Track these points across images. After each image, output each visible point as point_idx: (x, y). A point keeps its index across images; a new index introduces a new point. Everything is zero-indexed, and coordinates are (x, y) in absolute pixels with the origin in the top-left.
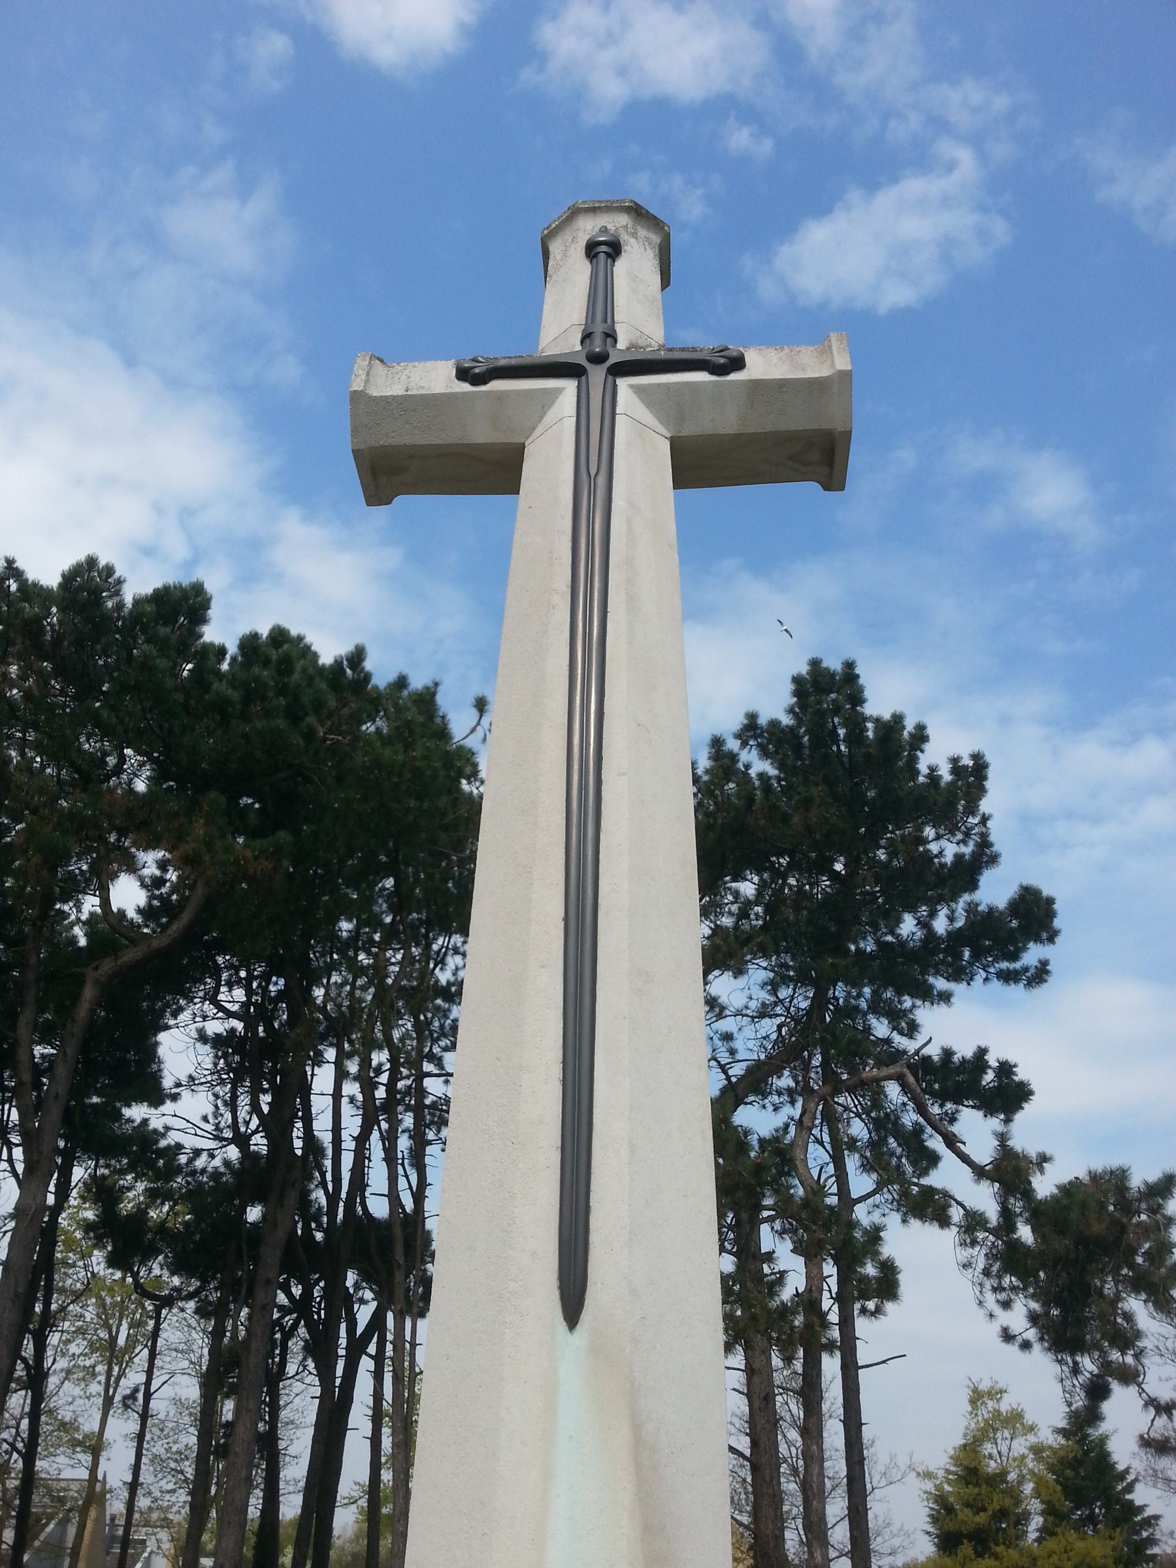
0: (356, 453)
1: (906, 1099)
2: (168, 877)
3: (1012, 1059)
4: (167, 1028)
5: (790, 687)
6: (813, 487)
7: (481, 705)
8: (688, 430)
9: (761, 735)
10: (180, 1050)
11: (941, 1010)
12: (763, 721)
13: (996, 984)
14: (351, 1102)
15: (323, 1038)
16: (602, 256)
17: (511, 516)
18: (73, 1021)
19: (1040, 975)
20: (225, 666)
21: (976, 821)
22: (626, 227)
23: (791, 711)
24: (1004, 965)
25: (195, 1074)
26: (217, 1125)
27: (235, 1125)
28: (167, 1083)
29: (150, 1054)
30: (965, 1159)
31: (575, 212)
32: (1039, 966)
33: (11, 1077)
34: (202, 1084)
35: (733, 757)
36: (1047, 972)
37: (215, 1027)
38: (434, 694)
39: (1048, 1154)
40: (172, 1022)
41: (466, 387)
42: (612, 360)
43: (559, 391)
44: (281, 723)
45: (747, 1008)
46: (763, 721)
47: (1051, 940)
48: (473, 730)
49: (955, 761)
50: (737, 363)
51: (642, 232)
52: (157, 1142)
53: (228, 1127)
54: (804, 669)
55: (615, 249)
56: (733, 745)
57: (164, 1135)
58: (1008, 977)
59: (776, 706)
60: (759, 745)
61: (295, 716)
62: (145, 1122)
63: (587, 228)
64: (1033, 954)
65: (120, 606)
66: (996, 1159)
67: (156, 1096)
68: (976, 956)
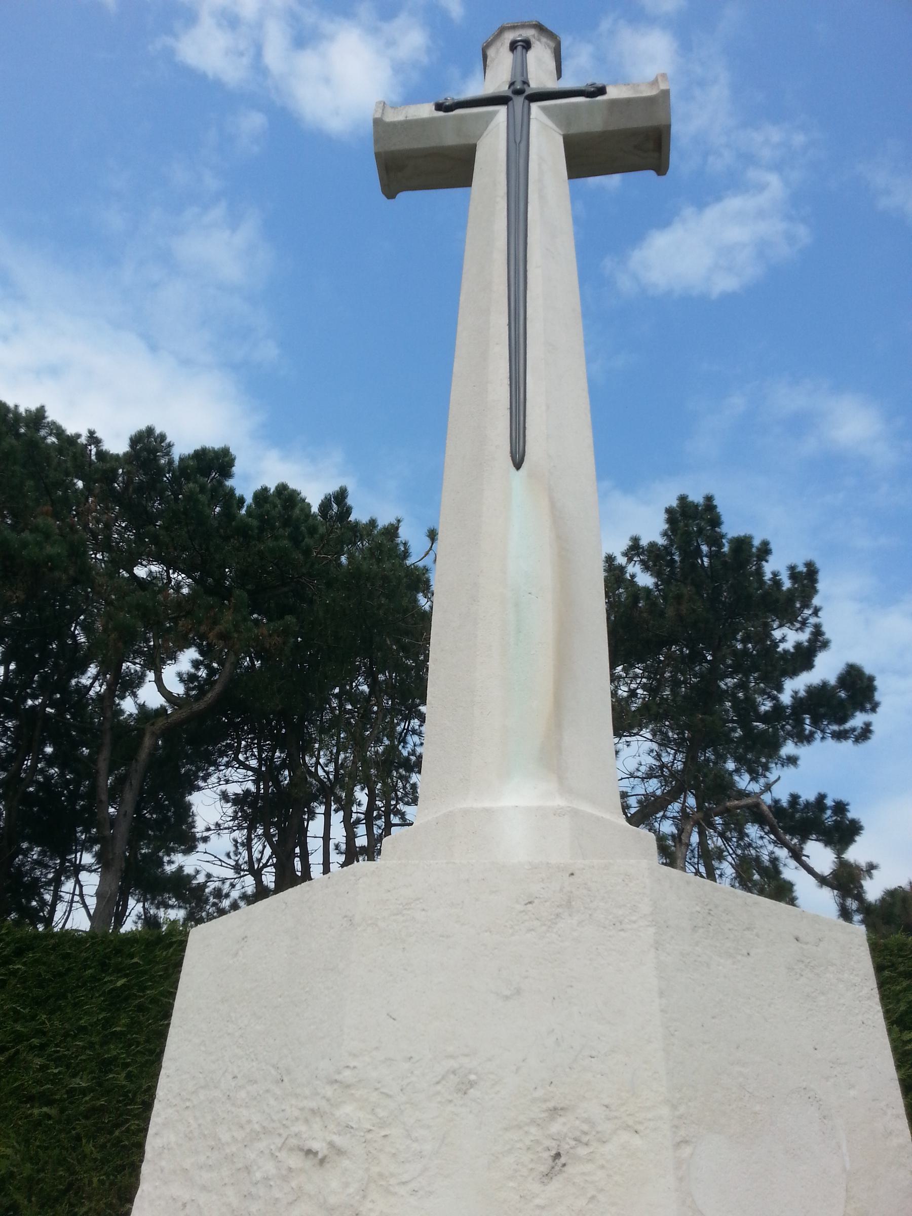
0: (378, 155)
1: (763, 834)
2: (200, 674)
4: (199, 789)
5: (663, 516)
6: (651, 174)
7: (433, 535)
8: (574, 130)
9: (643, 553)
10: (207, 806)
11: (790, 771)
12: (644, 542)
13: (830, 742)
14: (337, 849)
15: (315, 799)
16: (519, 48)
17: (468, 198)
18: (136, 760)
20: (243, 512)
21: (810, 612)
22: (534, 36)
23: (665, 534)
24: (835, 728)
25: (220, 822)
26: (237, 861)
27: (250, 861)
28: (199, 828)
29: (185, 813)
30: (810, 871)
31: (502, 30)
32: (864, 727)
33: (82, 833)
34: (226, 829)
35: (622, 569)
36: (870, 731)
37: (234, 789)
38: (397, 528)
39: (875, 862)
40: (201, 784)
41: (441, 114)
42: (526, 93)
43: (495, 113)
44: (286, 543)
45: (638, 770)
46: (644, 542)
47: (874, 709)
48: (427, 553)
49: (792, 568)
50: (602, 91)
51: (544, 40)
52: (190, 882)
53: (245, 862)
54: (674, 503)
55: (527, 45)
56: (621, 560)
57: (195, 877)
58: (840, 736)
59: (653, 530)
60: (641, 561)
61: (296, 540)
62: (181, 868)
63: (510, 36)
64: (858, 720)
65: (171, 462)
66: (834, 870)
67: (189, 843)
68: (815, 723)
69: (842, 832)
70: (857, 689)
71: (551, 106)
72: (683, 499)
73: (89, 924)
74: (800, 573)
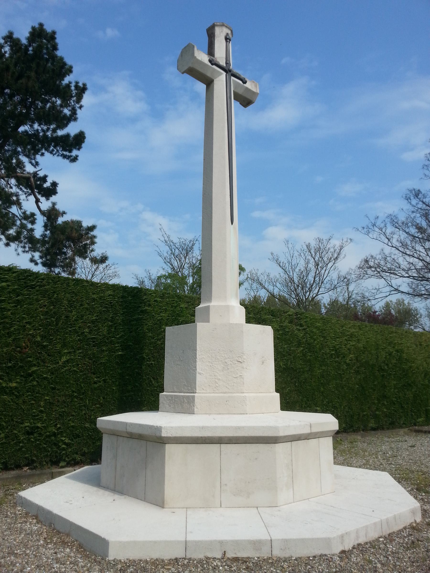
3: (57, 181)
36: (77, 159)
39: (66, 212)
41: (210, 64)
46: (15, 36)
49: (77, 83)
58: (64, 157)
64: (75, 153)
70: (79, 140)
71: (236, 81)
73: (336, 421)
74: (80, 87)
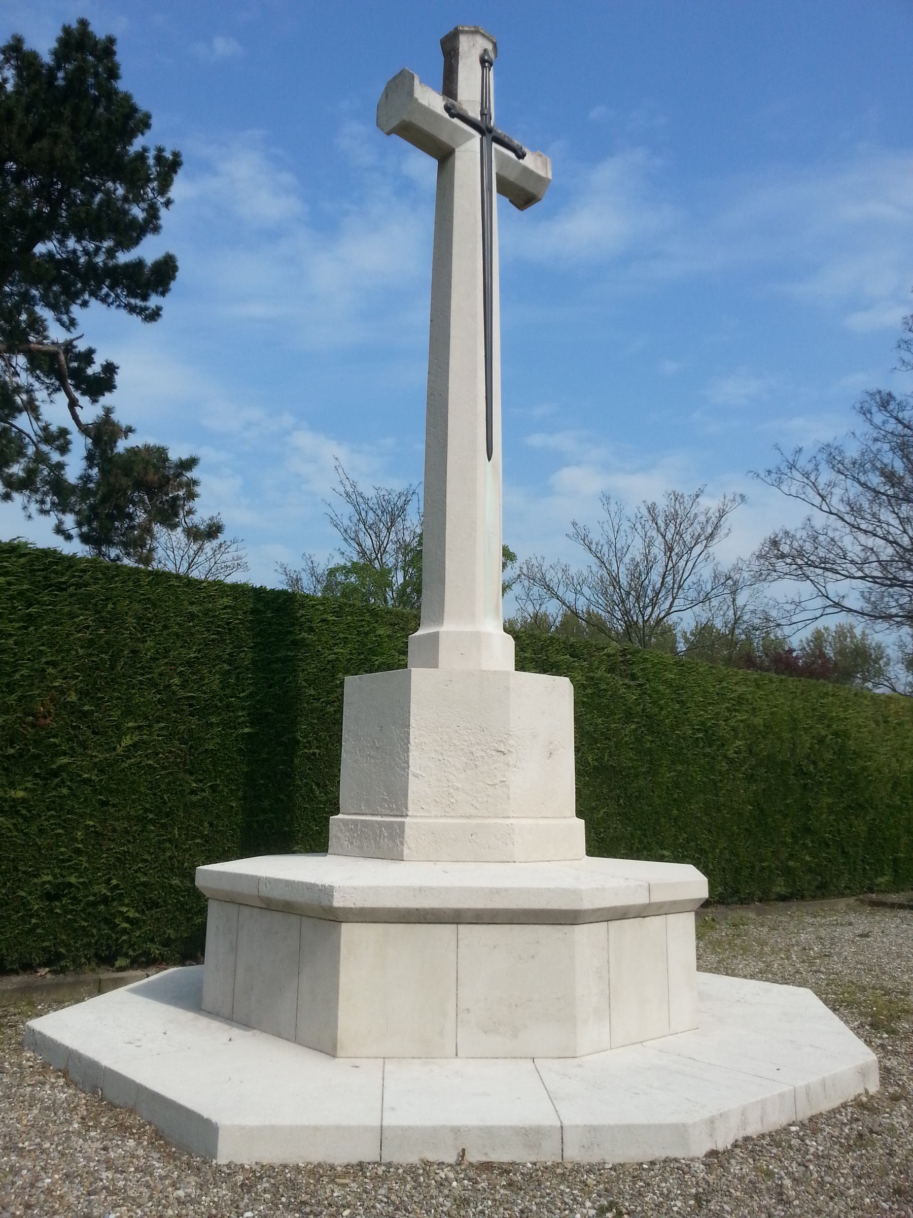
3: (116, 362)
19: (153, 315)
36: (158, 315)
41: (446, 115)
58: (132, 309)
64: (154, 301)
69: (104, 383)
70: (163, 273)
72: (83, 23)
73: (704, 879)
74: (166, 159)
